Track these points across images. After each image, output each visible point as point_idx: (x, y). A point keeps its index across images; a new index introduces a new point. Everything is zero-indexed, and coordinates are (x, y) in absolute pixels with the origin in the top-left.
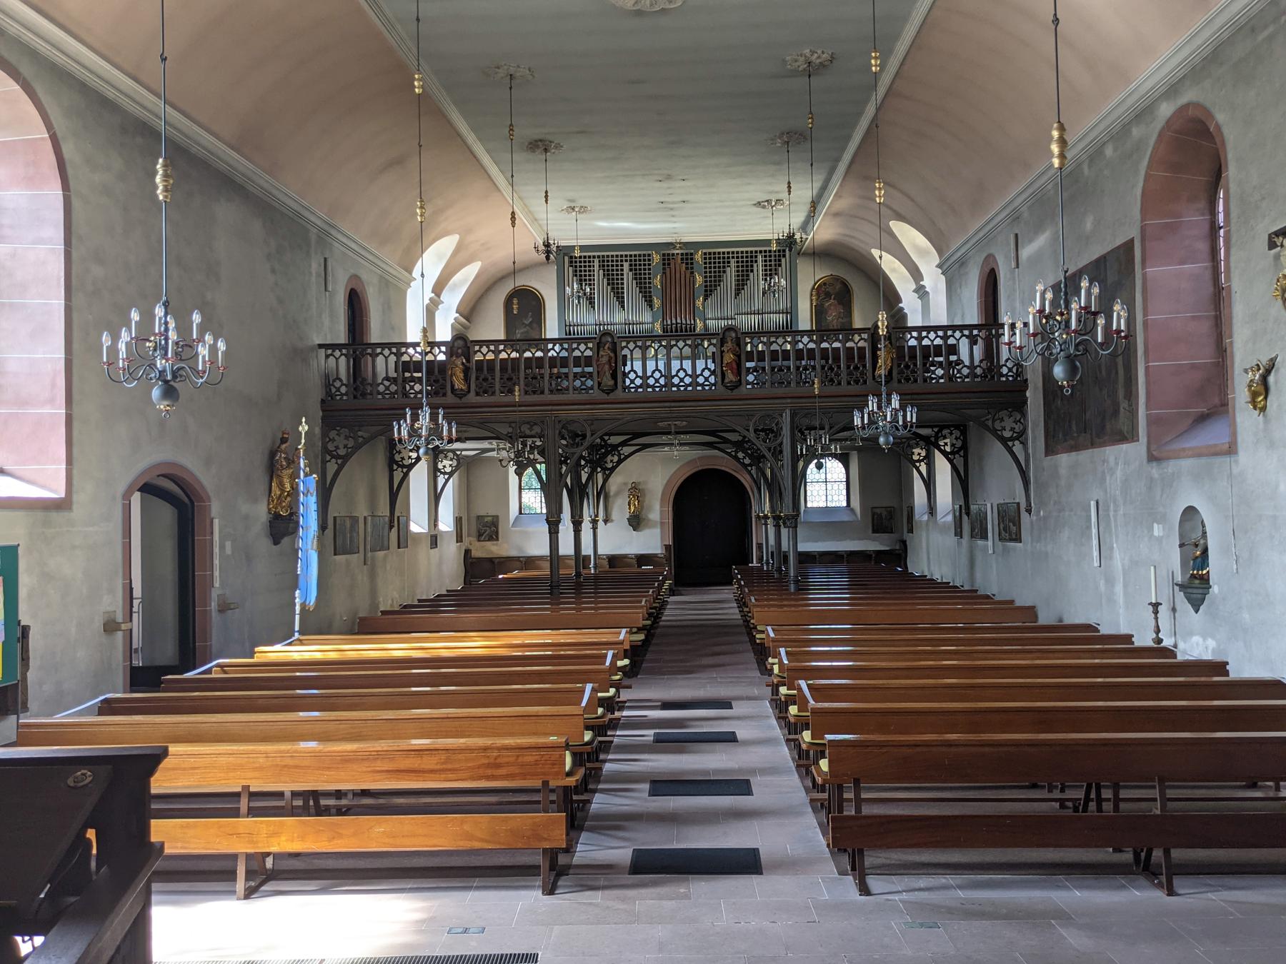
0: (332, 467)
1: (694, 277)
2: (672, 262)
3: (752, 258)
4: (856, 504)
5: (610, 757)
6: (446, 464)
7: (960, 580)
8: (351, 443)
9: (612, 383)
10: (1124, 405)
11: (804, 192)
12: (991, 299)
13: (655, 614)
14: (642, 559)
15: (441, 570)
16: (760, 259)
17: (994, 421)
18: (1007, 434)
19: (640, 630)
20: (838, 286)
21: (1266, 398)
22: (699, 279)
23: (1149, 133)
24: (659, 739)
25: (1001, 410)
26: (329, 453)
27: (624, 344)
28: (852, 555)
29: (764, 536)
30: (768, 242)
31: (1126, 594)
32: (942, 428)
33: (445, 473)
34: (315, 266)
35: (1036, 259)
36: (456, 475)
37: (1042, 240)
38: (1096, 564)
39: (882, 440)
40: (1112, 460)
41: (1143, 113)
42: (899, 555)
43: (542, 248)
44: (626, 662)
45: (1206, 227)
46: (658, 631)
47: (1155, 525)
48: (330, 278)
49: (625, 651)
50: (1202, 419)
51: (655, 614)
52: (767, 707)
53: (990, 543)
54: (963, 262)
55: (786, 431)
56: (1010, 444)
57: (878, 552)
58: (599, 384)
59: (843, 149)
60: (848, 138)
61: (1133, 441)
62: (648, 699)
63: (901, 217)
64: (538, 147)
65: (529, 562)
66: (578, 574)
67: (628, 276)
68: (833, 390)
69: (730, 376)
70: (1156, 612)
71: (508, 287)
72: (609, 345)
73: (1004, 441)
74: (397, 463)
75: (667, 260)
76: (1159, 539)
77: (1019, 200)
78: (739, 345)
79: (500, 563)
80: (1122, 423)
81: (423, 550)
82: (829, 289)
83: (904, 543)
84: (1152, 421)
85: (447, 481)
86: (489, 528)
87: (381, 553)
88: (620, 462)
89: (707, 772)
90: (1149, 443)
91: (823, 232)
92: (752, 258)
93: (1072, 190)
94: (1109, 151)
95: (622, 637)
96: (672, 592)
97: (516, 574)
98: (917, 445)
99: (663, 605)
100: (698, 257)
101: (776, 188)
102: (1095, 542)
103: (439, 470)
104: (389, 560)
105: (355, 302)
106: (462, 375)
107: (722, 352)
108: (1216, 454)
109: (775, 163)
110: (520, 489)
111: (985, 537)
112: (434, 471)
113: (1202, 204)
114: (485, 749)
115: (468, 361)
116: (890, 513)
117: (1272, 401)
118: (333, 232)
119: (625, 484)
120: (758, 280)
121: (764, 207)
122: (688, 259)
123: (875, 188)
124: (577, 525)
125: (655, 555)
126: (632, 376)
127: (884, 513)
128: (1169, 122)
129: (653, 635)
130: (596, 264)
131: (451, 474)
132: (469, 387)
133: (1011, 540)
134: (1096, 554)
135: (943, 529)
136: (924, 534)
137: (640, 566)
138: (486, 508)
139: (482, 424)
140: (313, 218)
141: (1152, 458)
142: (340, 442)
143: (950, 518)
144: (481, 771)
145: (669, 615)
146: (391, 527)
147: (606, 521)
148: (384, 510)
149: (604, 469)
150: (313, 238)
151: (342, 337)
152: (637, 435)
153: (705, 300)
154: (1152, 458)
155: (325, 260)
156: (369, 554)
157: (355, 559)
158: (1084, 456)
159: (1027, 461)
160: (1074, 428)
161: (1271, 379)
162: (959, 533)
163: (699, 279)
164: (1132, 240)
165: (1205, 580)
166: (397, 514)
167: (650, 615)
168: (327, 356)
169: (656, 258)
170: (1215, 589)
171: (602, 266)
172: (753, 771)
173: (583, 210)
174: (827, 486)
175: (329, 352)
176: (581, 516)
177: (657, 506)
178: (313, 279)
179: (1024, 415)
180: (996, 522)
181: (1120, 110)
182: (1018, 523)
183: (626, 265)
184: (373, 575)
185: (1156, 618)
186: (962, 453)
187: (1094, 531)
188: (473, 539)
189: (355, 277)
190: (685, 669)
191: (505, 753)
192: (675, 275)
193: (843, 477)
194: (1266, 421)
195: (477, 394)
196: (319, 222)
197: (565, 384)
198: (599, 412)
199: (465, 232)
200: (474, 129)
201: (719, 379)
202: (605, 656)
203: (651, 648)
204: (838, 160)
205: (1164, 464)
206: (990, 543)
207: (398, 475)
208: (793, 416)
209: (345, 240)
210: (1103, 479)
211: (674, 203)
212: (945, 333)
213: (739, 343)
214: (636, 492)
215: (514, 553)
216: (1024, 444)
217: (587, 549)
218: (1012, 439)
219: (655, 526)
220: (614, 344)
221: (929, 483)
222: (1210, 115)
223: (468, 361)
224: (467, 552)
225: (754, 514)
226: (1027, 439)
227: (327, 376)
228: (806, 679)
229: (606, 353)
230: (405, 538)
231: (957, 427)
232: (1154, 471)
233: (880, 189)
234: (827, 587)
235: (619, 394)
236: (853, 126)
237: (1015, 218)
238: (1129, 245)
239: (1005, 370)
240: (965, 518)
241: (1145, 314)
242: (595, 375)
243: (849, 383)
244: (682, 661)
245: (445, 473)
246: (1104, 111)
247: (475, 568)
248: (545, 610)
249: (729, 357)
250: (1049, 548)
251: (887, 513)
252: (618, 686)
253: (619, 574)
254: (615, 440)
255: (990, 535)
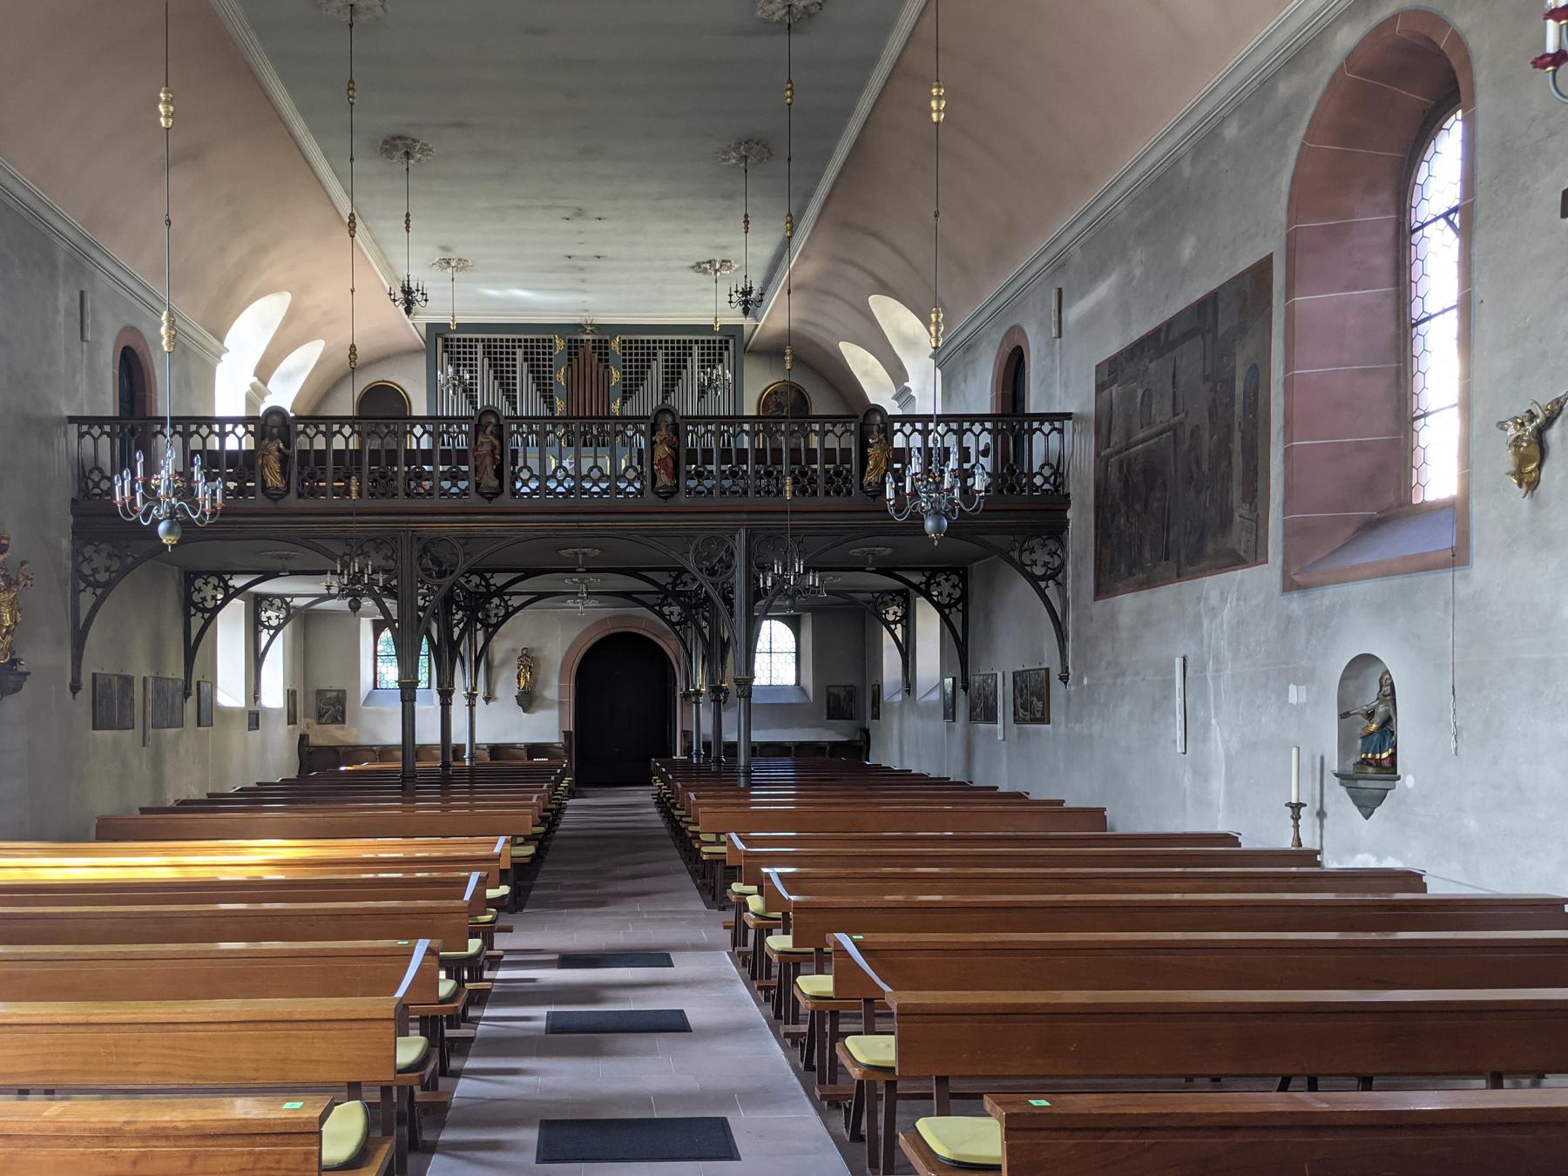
0: (87, 600)
1: (610, 373)
2: (580, 351)
3: (686, 348)
4: (808, 682)
5: (471, 1063)
6: (271, 616)
7: (955, 774)
8: (115, 565)
9: (495, 483)
10: (1240, 511)
11: (758, 249)
12: (1010, 392)
13: (551, 818)
14: (533, 750)
15: (273, 756)
16: (696, 351)
17: (1021, 552)
18: (1039, 571)
19: (528, 840)
20: (793, 396)
21: (1539, 467)
22: (616, 376)
23: (1314, 83)
24: (557, 1026)
25: (1031, 538)
26: (84, 578)
27: (514, 427)
28: (801, 746)
29: (697, 722)
30: (707, 329)
31: (1229, 793)
32: (935, 572)
33: (270, 627)
34: (65, 298)
35: (1092, 320)
36: (288, 627)
37: (1103, 290)
38: (1180, 749)
39: (929, 524)
40: (1214, 597)
41: (1296, 58)
42: (858, 749)
43: (400, 295)
44: (504, 890)
45: (1389, 230)
46: (554, 842)
47: (1292, 687)
48: (88, 321)
49: (503, 872)
50: (1371, 526)
51: (551, 818)
52: (725, 964)
53: (999, 726)
54: (969, 346)
55: (740, 560)
56: (1043, 584)
57: (835, 745)
58: (478, 485)
59: (819, 176)
60: (827, 155)
61: (1256, 563)
62: (540, 948)
63: (886, 289)
64: (395, 147)
65: (384, 752)
66: (446, 765)
67: (521, 367)
68: (806, 502)
69: (664, 479)
70: (1296, 818)
71: (364, 382)
72: (487, 424)
73: (1034, 580)
74: (195, 605)
75: (574, 348)
76: (1299, 709)
77: (1068, 237)
78: (676, 434)
79: (345, 753)
80: (1238, 538)
81: (238, 734)
82: (781, 399)
83: (866, 732)
84: (1293, 532)
85: (272, 638)
86: (333, 707)
87: (171, 732)
88: (507, 615)
89: (643, 1100)
90: (1286, 562)
91: (774, 317)
92: (686, 348)
93: (1166, 200)
94: (1231, 131)
95: (497, 849)
96: (572, 794)
97: (365, 765)
98: (886, 605)
99: (559, 811)
100: (615, 345)
101: (723, 239)
102: (1180, 717)
103: (262, 623)
104: (182, 742)
105: (133, 369)
106: (277, 467)
107: (653, 443)
108: (1426, 568)
109: (726, 197)
110: (375, 655)
111: (991, 717)
112: (255, 625)
113: (1386, 197)
114: (110, 1136)
115: (287, 446)
116: (850, 694)
117: (1552, 474)
118: (95, 254)
119: (514, 650)
120: (694, 373)
121: (705, 271)
122: (602, 348)
123: (931, 97)
124: (446, 696)
125: (551, 745)
126: (525, 475)
127: (843, 694)
128: (1351, 57)
129: (546, 848)
130: (480, 350)
131: (278, 629)
132: (288, 484)
133: (1034, 721)
134: (1180, 734)
135: (925, 711)
136: (896, 720)
137: (530, 758)
138: (330, 680)
139: (308, 541)
140: (60, 225)
141: (1290, 585)
142: (99, 561)
143: (936, 696)
144: (1118, 421)
145: (569, 820)
146: (187, 695)
147: (487, 699)
148: (174, 669)
149: (486, 625)
150: (61, 257)
151: (108, 405)
152: (529, 573)
153: (623, 403)
154: (1290, 585)
155: (82, 294)
156: (151, 732)
157: (126, 736)
158: (1163, 595)
159: (1064, 613)
160: (1147, 555)
161: (1553, 435)
162: (950, 712)
163: (616, 376)
164: (1269, 260)
165: (1390, 769)
166: (195, 677)
167: (544, 819)
168: (81, 435)
169: (560, 345)
170: (1408, 780)
171: (487, 353)
172: (728, 1098)
173: (462, 265)
174: (777, 656)
175: (85, 428)
176: (452, 684)
177: (554, 682)
178: (61, 318)
179: (1063, 545)
180: (1010, 698)
181: (1261, 56)
182: (1044, 695)
183: (519, 353)
184: (157, 762)
185: (1297, 827)
186: (960, 606)
187: (1179, 701)
188: (311, 721)
189: (131, 330)
190: (595, 901)
191: (161, 1148)
192: (587, 367)
193: (792, 646)
194: (1537, 505)
195: (300, 496)
196: (70, 234)
197: (427, 484)
198: (479, 525)
199: (300, 291)
200: (304, 112)
201: (648, 483)
202: (466, 881)
203: (545, 868)
204: (809, 195)
205: (1315, 593)
206: (999, 726)
207: (197, 622)
208: (750, 538)
209: (114, 270)
210: (1197, 623)
211: (584, 258)
212: (961, 426)
213: (675, 429)
214: (529, 661)
215: (365, 740)
216: (1061, 585)
217: (459, 736)
218: (1045, 578)
219: (550, 707)
220: (500, 427)
221: (907, 650)
222: (1437, 21)
223: (287, 446)
224: (303, 738)
225: (679, 693)
226: (1065, 578)
227: (80, 464)
228: (849, 931)
229: (487, 439)
230: (207, 713)
231: (954, 571)
232: (1294, 605)
233: (939, 98)
234: (769, 783)
235: (505, 500)
236: (837, 134)
237: (1059, 265)
238: (1264, 266)
239: (1038, 481)
240: (961, 693)
241: (1289, 364)
242: (472, 474)
243: (827, 493)
244: (586, 886)
245: (270, 627)
246: (1232, 62)
247: (308, 754)
248: (392, 809)
249: (663, 451)
250: (1096, 728)
251: (846, 693)
252: (486, 933)
253: (503, 767)
254: (499, 580)
255: (1000, 715)
